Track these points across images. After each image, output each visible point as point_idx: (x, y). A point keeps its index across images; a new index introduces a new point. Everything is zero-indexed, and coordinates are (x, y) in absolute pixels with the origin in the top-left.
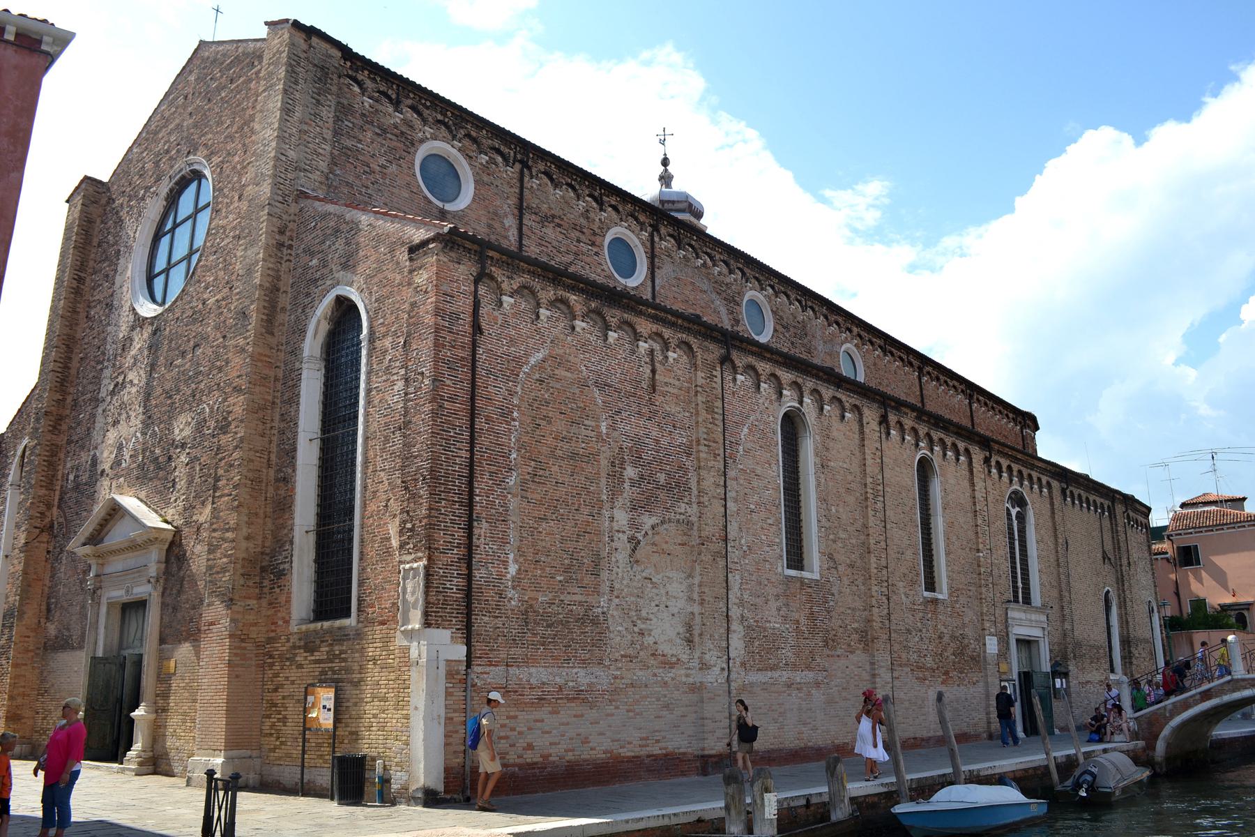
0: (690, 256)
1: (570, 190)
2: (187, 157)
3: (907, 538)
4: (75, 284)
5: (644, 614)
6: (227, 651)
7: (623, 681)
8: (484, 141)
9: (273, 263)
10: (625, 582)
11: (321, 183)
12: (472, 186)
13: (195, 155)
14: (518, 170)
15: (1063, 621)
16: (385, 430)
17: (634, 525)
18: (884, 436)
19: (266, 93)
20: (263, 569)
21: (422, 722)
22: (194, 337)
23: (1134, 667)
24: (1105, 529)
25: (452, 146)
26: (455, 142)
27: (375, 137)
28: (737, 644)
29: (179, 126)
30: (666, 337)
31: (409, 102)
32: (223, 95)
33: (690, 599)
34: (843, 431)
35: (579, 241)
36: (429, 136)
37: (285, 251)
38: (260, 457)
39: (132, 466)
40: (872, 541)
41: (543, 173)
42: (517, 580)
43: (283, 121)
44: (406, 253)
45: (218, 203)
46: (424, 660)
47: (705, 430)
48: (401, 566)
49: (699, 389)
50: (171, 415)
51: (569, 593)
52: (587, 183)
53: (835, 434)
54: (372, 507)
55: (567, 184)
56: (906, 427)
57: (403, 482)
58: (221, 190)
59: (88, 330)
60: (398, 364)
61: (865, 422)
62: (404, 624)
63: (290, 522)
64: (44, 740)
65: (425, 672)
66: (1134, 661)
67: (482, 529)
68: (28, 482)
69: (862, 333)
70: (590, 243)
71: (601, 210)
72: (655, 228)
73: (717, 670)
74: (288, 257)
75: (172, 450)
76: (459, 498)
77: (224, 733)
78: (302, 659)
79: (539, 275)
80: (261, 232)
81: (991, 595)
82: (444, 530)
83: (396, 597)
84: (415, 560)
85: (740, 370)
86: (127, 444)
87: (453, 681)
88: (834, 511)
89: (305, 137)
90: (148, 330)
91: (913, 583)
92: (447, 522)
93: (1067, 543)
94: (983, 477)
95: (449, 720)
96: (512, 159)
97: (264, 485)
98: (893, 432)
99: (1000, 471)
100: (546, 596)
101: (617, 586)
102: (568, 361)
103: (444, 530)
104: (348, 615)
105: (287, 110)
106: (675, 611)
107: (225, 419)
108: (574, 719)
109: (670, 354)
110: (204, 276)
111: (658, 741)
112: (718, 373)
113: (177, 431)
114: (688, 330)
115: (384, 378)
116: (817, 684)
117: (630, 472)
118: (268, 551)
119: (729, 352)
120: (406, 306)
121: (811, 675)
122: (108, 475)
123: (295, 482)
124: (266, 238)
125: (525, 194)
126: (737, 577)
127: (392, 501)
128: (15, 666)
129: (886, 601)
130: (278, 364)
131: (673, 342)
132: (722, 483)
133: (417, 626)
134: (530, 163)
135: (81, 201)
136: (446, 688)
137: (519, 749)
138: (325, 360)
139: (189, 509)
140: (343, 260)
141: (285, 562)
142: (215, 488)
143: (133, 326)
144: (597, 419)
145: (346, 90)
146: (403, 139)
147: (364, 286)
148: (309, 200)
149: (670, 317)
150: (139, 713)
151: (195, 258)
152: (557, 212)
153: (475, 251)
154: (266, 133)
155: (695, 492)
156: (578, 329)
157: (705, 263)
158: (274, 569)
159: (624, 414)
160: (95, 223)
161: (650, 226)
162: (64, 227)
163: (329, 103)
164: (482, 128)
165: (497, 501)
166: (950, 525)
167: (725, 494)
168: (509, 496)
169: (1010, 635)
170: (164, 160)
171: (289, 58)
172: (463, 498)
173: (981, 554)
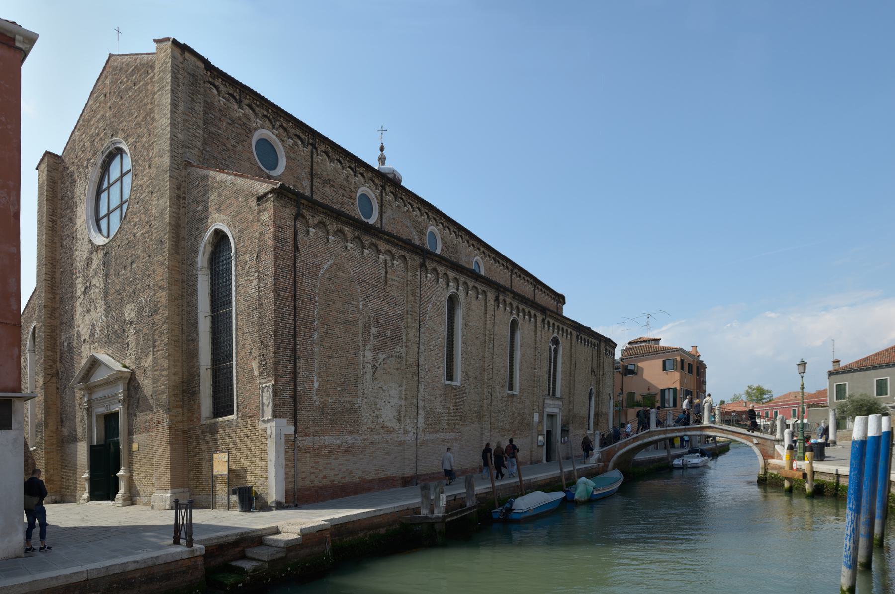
0: (401, 205)
1: (338, 163)
2: (112, 138)
3: (502, 363)
4: (51, 224)
5: (378, 406)
6: (168, 437)
7: (368, 441)
8: (291, 130)
9: (175, 209)
10: (370, 390)
11: (199, 156)
12: (285, 160)
13: (117, 137)
14: (310, 150)
15: (570, 404)
16: (247, 309)
17: (375, 359)
18: (496, 308)
19: (160, 93)
20: (184, 391)
21: (274, 467)
22: (131, 257)
23: (599, 427)
24: (594, 356)
25: (273, 133)
26: (274, 130)
27: (228, 126)
28: (421, 420)
29: (103, 116)
30: (393, 252)
31: (247, 102)
32: (130, 94)
33: (400, 398)
34: (477, 306)
35: (343, 196)
36: (259, 126)
37: (182, 201)
38: (178, 328)
39: (102, 336)
40: (486, 365)
41: (324, 152)
42: (318, 390)
43: (172, 112)
44: (255, 201)
45: (135, 170)
46: (274, 435)
47: (411, 306)
48: (260, 385)
49: (409, 282)
50: (122, 303)
51: (343, 397)
52: (348, 159)
53: (473, 307)
54: (243, 354)
55: (337, 159)
56: (507, 302)
57: (259, 339)
58: (137, 161)
59: (63, 254)
60: (253, 270)
61: (488, 300)
62: (263, 417)
63: (197, 364)
64: (68, 492)
65: (275, 442)
66: (599, 424)
67: (301, 364)
68: (40, 348)
69: (485, 251)
70: (349, 197)
71: (355, 176)
72: (384, 188)
73: (411, 434)
74: (184, 205)
75: (125, 326)
76: (289, 346)
77: (169, 480)
78: (208, 438)
79: (328, 215)
80: (166, 189)
81: (538, 392)
82: (282, 365)
83: (258, 402)
84: (268, 382)
85: (429, 271)
86: (97, 323)
87: (289, 445)
88: (469, 349)
89: (187, 124)
90: (101, 254)
91: (503, 386)
92: (283, 360)
93: (576, 364)
94: (541, 329)
95: (287, 466)
96: (306, 142)
97: (181, 343)
98: (501, 305)
99: (549, 326)
100: (332, 399)
101: (366, 392)
102: (343, 267)
103: (282, 365)
104: (232, 413)
105: (174, 105)
106: (392, 404)
107: (156, 306)
108: (345, 462)
109: (395, 262)
110: (132, 218)
111: (383, 471)
112: (418, 273)
113: (126, 315)
114: (404, 248)
115: (246, 278)
116: (456, 439)
117: (374, 330)
118: (186, 381)
119: (424, 261)
120: (257, 235)
121: (454, 435)
122: (87, 342)
123: (198, 341)
124: (170, 192)
125: (314, 165)
126: (423, 385)
127: (253, 350)
128: (46, 453)
129: (490, 396)
130: (184, 272)
131: (397, 255)
132: (418, 335)
133: (270, 417)
134: (317, 145)
135: (46, 169)
136: (285, 449)
137: (321, 478)
138: (211, 269)
139: (138, 359)
140: (217, 206)
141: (196, 387)
142: (154, 347)
143: (91, 251)
144: (358, 301)
145: (209, 92)
146: (244, 128)
147: (231, 223)
148: (193, 168)
149: (396, 240)
150: (120, 473)
151: (125, 207)
152: (332, 178)
153: (294, 200)
154: (163, 120)
155: (404, 340)
156: (348, 248)
157: (408, 209)
158: (190, 390)
159: (371, 297)
160: (57, 183)
161: (381, 186)
162: (37, 187)
163: (199, 101)
164: (290, 121)
165: (308, 348)
166: (523, 356)
167: (419, 341)
168: (314, 345)
169: (545, 412)
170: (97, 140)
171: (172, 67)
172: (291, 347)
173: (536, 371)
